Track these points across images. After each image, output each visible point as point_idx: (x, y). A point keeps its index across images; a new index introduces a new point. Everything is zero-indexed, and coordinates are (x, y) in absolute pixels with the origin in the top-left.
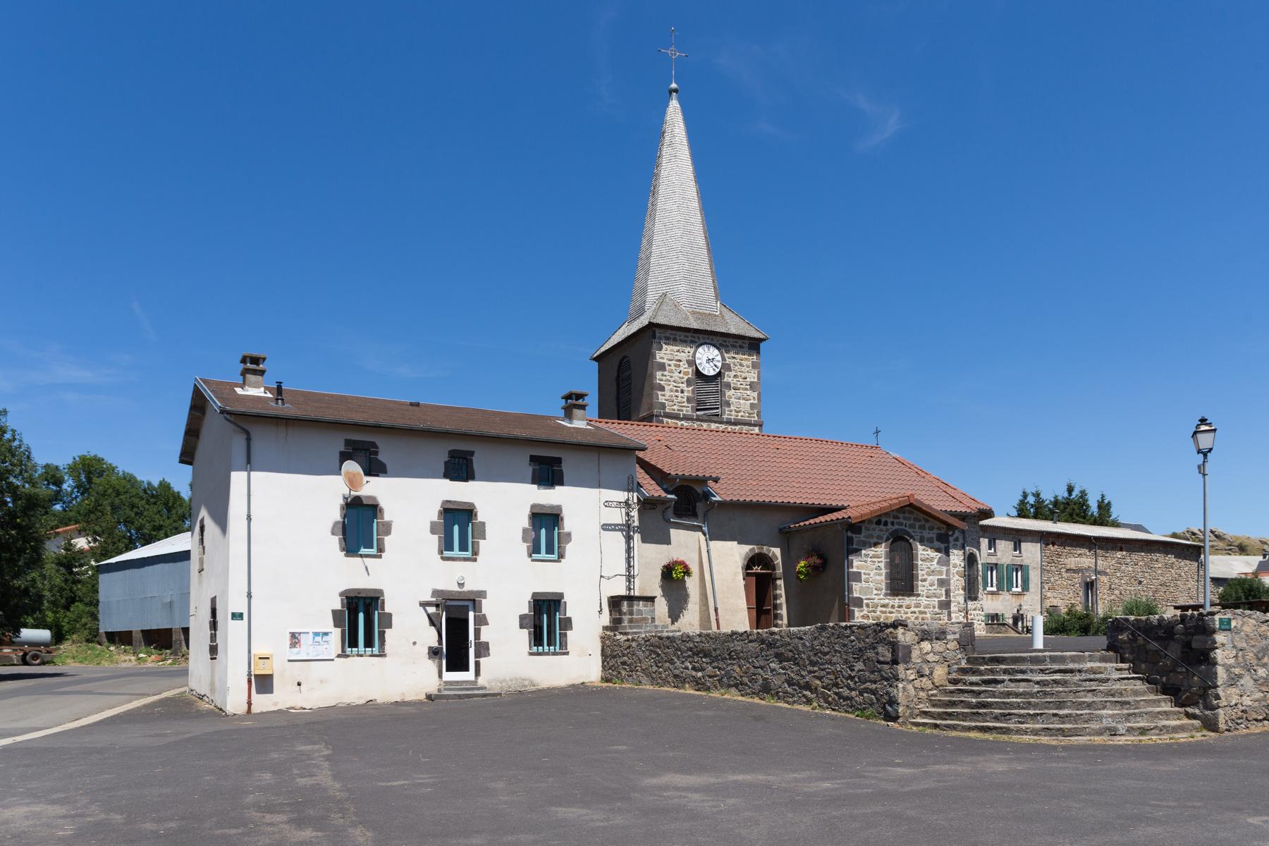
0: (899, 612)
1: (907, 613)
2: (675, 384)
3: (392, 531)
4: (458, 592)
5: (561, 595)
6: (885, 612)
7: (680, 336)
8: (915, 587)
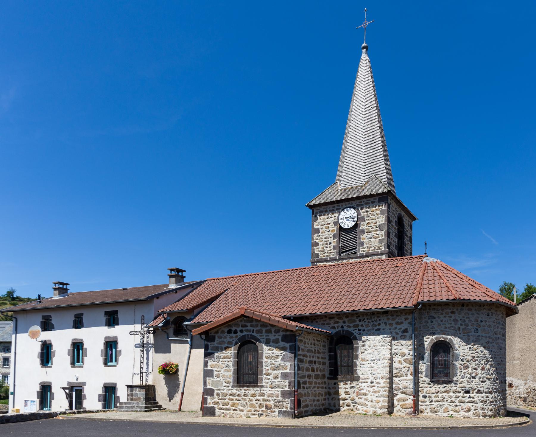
0: (245, 400)
1: (251, 401)
2: (326, 240)
3: (56, 355)
4: (76, 383)
5: (115, 384)
6: (232, 400)
7: (330, 208)
8: (259, 381)
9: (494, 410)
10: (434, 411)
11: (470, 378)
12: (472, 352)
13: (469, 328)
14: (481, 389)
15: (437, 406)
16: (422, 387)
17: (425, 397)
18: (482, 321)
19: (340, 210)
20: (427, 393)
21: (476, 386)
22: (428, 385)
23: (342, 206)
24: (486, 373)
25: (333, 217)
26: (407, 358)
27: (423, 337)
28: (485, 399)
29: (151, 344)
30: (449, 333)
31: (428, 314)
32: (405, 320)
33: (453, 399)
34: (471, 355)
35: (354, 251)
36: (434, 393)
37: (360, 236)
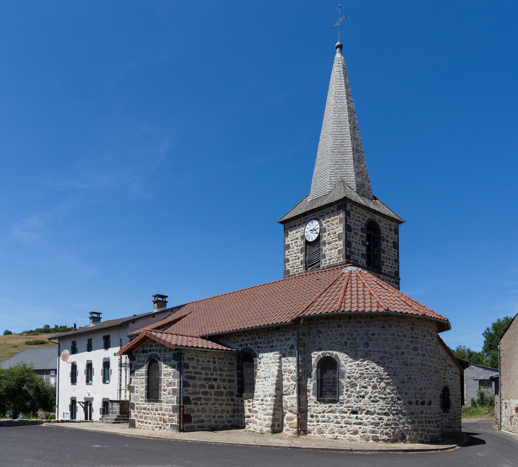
7: (298, 222)
9: (392, 434)
10: (320, 432)
11: (357, 397)
12: (360, 368)
13: (357, 342)
14: (372, 410)
15: (323, 426)
16: (310, 406)
17: (312, 416)
18: (373, 334)
19: (306, 223)
20: (314, 413)
21: (365, 406)
22: (315, 404)
23: (307, 219)
24: (380, 392)
25: (301, 231)
26: (293, 375)
27: (311, 353)
28: (377, 421)
29: (128, 364)
30: (335, 348)
31: (315, 329)
32: (292, 336)
33: (339, 420)
34: (359, 372)
35: (318, 264)
36: (320, 413)
37: (322, 248)
